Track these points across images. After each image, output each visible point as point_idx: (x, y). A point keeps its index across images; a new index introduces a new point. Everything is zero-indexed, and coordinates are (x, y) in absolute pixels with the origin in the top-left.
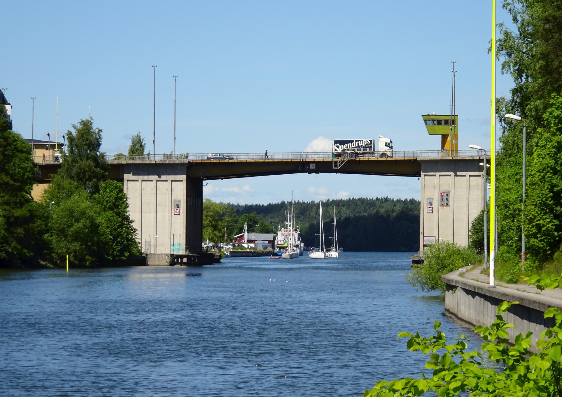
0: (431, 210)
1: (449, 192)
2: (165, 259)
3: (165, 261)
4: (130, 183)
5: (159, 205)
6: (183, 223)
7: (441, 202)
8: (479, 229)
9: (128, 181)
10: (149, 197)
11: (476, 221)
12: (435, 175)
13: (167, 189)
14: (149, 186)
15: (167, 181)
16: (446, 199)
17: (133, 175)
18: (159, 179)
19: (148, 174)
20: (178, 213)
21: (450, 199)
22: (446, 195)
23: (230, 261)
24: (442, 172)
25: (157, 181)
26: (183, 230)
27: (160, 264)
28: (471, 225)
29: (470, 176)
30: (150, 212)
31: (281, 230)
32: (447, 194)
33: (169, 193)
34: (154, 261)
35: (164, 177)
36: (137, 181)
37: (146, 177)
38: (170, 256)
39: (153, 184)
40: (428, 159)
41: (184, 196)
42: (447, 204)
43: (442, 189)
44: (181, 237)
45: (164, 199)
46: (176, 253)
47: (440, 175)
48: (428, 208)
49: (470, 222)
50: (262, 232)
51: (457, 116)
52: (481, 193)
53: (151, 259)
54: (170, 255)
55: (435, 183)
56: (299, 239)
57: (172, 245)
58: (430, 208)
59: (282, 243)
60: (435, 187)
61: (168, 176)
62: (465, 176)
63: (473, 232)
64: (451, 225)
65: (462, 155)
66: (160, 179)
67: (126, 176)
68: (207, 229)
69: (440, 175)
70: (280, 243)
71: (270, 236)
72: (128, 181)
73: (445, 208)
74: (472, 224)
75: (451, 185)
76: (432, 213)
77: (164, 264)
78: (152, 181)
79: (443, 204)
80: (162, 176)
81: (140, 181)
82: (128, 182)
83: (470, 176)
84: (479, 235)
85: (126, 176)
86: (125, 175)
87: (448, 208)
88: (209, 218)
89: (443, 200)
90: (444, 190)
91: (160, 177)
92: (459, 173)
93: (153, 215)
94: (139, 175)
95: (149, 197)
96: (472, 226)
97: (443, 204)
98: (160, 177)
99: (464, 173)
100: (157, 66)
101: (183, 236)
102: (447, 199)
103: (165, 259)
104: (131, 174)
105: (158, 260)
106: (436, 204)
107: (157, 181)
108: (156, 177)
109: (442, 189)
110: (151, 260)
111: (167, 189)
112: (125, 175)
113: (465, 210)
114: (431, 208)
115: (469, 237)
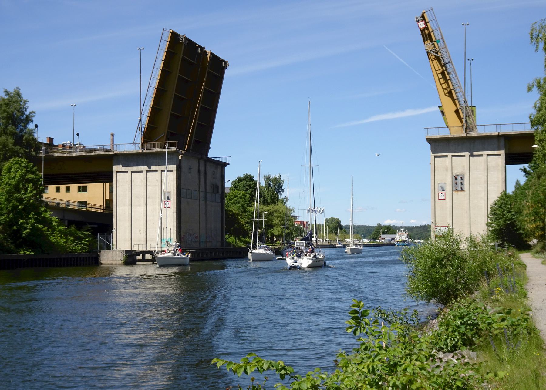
0: (443, 196)
1: (464, 175)
2: (119, 257)
3: (119, 259)
4: (120, 175)
5: (148, 198)
6: (174, 217)
7: (455, 186)
8: (500, 215)
9: (117, 172)
10: (139, 190)
11: (496, 204)
12: (446, 156)
13: (157, 180)
14: (139, 178)
15: (156, 171)
16: (460, 183)
17: (123, 166)
18: (148, 169)
19: (138, 165)
20: (168, 206)
21: (465, 183)
22: (460, 178)
23: (375, 249)
24: (455, 152)
25: (147, 171)
26: (174, 224)
27: (113, 263)
28: (490, 210)
29: (488, 155)
30: (139, 206)
31: (398, 233)
32: (461, 178)
33: (158, 184)
34: (108, 259)
35: (153, 168)
36: (127, 172)
37: (135, 168)
38: (124, 253)
39: (143, 175)
40: (438, 137)
41: (174, 187)
42: (462, 188)
43: (456, 172)
44: (172, 231)
45: (154, 190)
46: (136, 248)
47: (453, 156)
48: (440, 194)
49: (489, 206)
50: (392, 234)
51: (475, 107)
52: (502, 175)
53: (104, 256)
54: (125, 252)
55: (447, 164)
56: (407, 237)
57: (162, 240)
58: (442, 193)
59: (399, 239)
60: (447, 170)
61: (157, 166)
62: (481, 155)
63: (493, 219)
64: (467, 212)
65: (481, 131)
66: (150, 170)
67: (116, 168)
68: (277, 227)
69: (453, 156)
70: (397, 239)
71: (393, 236)
72: (117, 172)
73: (459, 193)
74: (491, 208)
75: (465, 166)
76: (445, 199)
77: (118, 263)
78: (141, 172)
79: (456, 189)
80: (152, 167)
81: (129, 173)
82: (118, 174)
83: (488, 155)
84: (500, 222)
85: (116, 168)
86: (114, 166)
87: (463, 193)
88: (279, 219)
89: (456, 184)
90: (458, 173)
91: (150, 168)
92: (475, 153)
93: (143, 208)
94: (128, 166)
95: (139, 190)
96: (491, 211)
97: (456, 189)
98: (150, 168)
99: (480, 153)
100: (143, 49)
101: (173, 230)
102: (461, 183)
103: (119, 257)
104: (121, 166)
105: (112, 258)
106: (448, 189)
107: (147, 171)
108: (146, 168)
109: (455, 172)
110: (105, 258)
111: (157, 180)
112: (114, 166)
113: (483, 194)
114: (443, 194)
115: (488, 225)
